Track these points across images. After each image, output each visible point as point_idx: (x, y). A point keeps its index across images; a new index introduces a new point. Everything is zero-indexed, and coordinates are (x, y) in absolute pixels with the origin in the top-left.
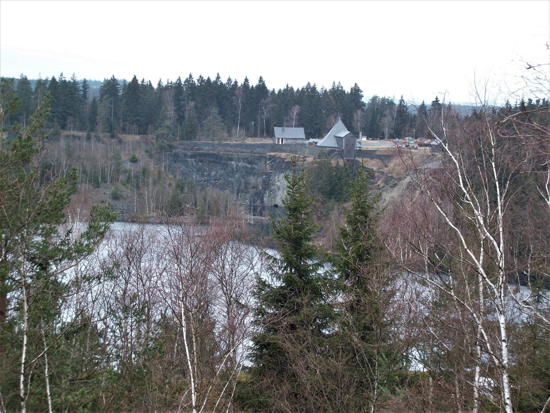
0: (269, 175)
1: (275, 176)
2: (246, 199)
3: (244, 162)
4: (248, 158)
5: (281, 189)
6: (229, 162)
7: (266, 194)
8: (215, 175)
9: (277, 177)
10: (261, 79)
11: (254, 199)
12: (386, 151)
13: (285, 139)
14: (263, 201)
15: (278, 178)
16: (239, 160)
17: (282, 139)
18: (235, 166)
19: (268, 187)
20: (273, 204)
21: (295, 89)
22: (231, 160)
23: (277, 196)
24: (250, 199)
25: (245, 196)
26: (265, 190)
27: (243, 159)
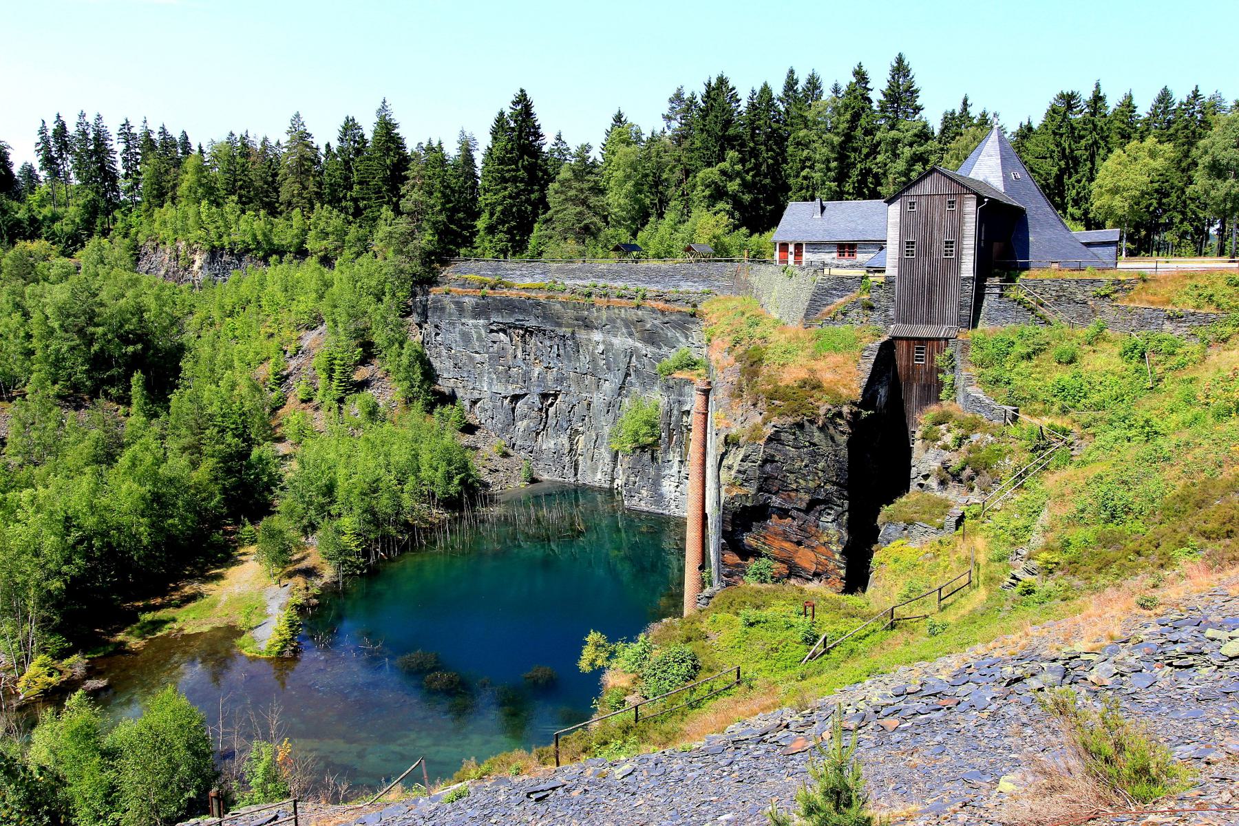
3: (631, 335)
6: (582, 335)
8: (541, 379)
13: (809, 244)
16: (610, 326)
17: (798, 246)
22: (588, 325)
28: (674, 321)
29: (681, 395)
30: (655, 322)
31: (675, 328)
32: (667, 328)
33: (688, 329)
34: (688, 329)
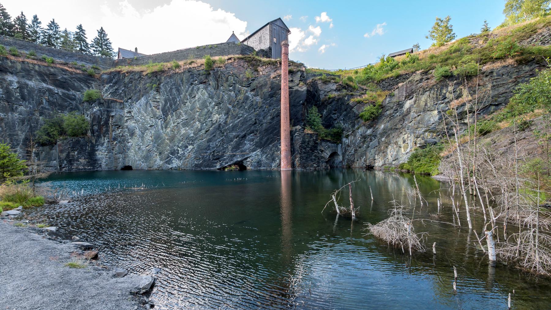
0: (107, 105)
1: (122, 108)
2: (50, 160)
4: (53, 74)
5: (138, 132)
7: (103, 144)
9: (126, 110)
10: (102, 32)
11: (68, 156)
12: (286, 141)
14: (95, 161)
15: (130, 112)
16: (27, 72)
18: (15, 85)
19: (107, 131)
20: (120, 165)
21: (166, 5)
23: (129, 149)
24: (59, 158)
25: (48, 153)
26: (99, 137)
27: (40, 74)
28: (79, 78)
29: (109, 108)
30: (65, 76)
31: (80, 81)
32: (75, 81)
33: (89, 83)
34: (89, 83)
